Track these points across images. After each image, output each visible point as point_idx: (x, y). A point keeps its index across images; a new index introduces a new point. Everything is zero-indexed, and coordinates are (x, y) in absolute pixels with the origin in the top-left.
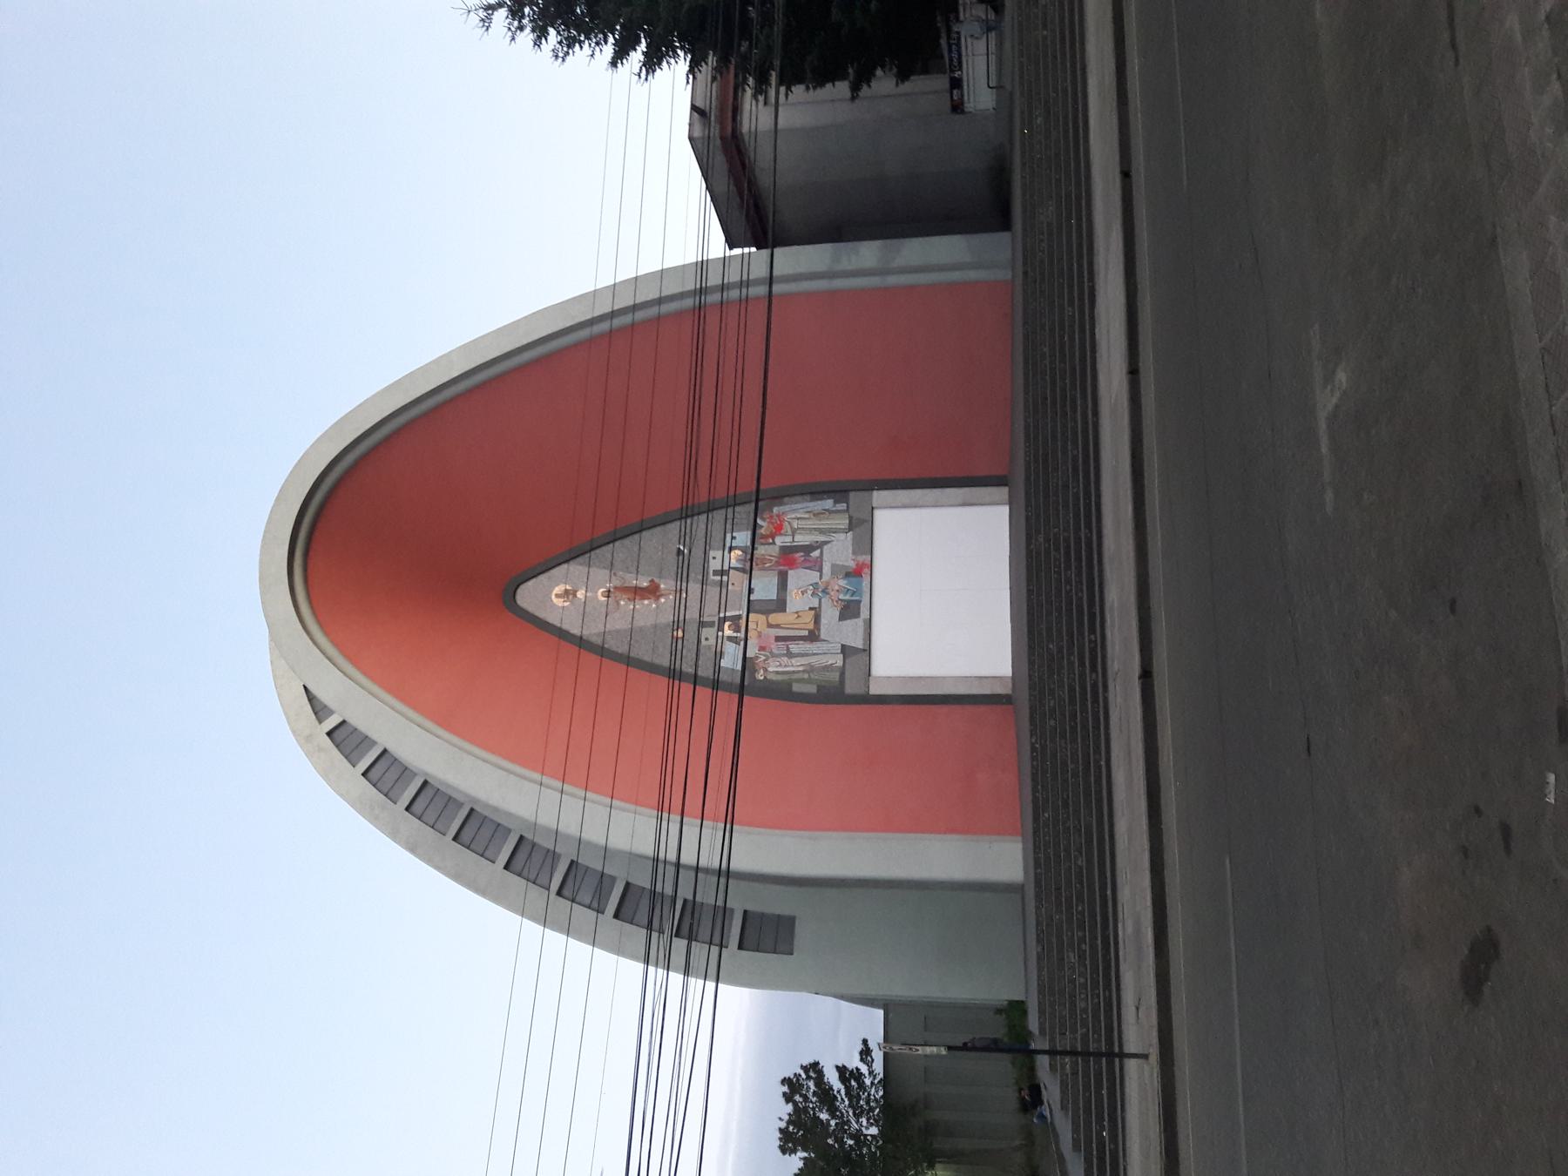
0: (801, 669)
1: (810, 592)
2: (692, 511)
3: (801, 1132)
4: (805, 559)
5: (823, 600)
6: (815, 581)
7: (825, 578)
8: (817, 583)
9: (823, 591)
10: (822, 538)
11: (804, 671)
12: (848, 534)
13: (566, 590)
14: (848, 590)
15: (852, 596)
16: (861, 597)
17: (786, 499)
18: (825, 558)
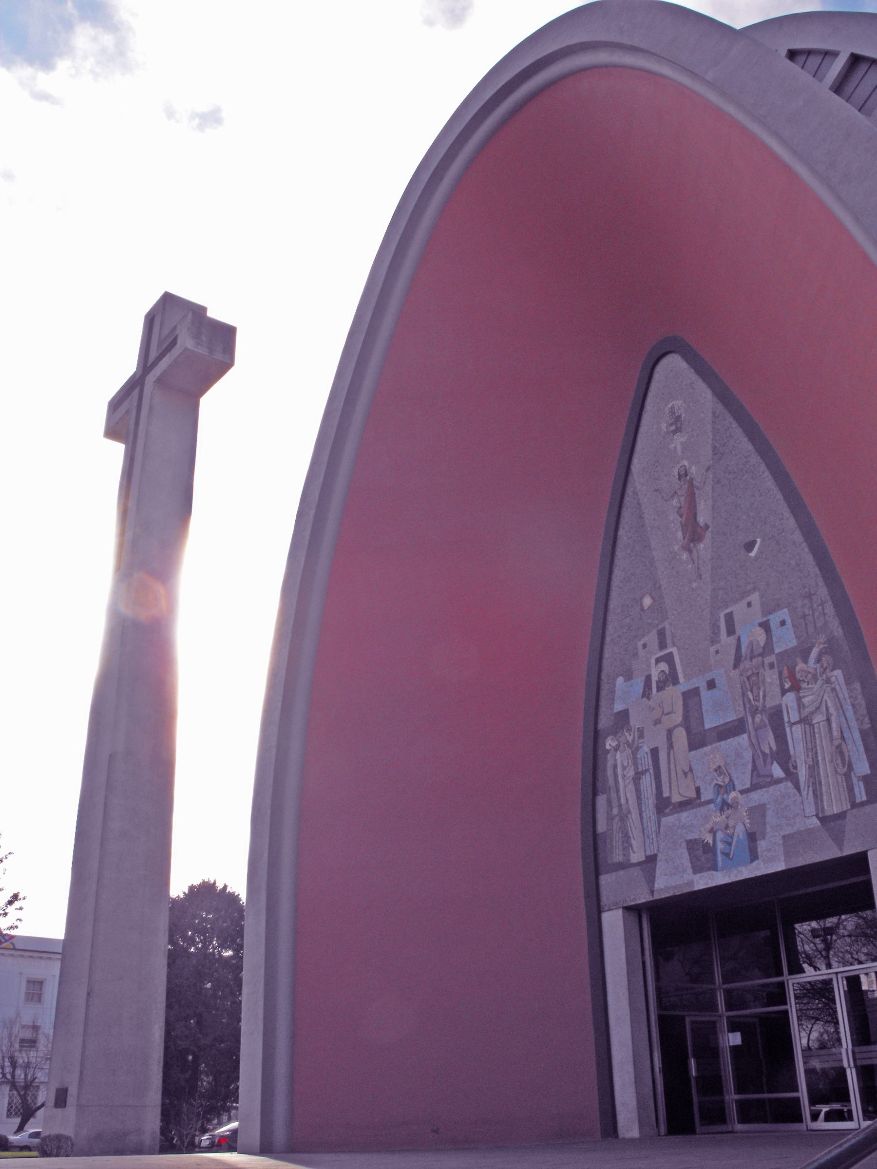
0: (623, 801)
14: (730, 844)
16: (722, 870)
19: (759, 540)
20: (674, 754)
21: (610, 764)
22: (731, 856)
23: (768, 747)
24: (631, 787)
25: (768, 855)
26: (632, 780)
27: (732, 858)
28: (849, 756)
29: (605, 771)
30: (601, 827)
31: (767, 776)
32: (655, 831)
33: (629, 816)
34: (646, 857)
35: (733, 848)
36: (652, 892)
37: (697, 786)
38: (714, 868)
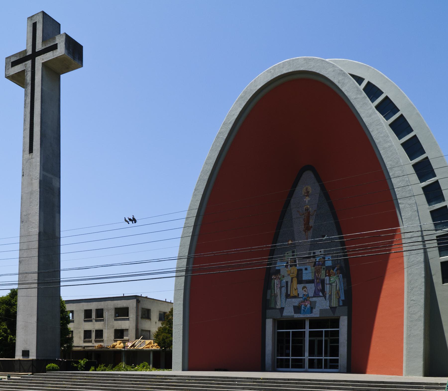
4: (319, 290)
10: (327, 296)
11: (275, 293)
14: (305, 309)
16: (302, 314)
24: (279, 289)
33: (277, 297)
37: (298, 293)
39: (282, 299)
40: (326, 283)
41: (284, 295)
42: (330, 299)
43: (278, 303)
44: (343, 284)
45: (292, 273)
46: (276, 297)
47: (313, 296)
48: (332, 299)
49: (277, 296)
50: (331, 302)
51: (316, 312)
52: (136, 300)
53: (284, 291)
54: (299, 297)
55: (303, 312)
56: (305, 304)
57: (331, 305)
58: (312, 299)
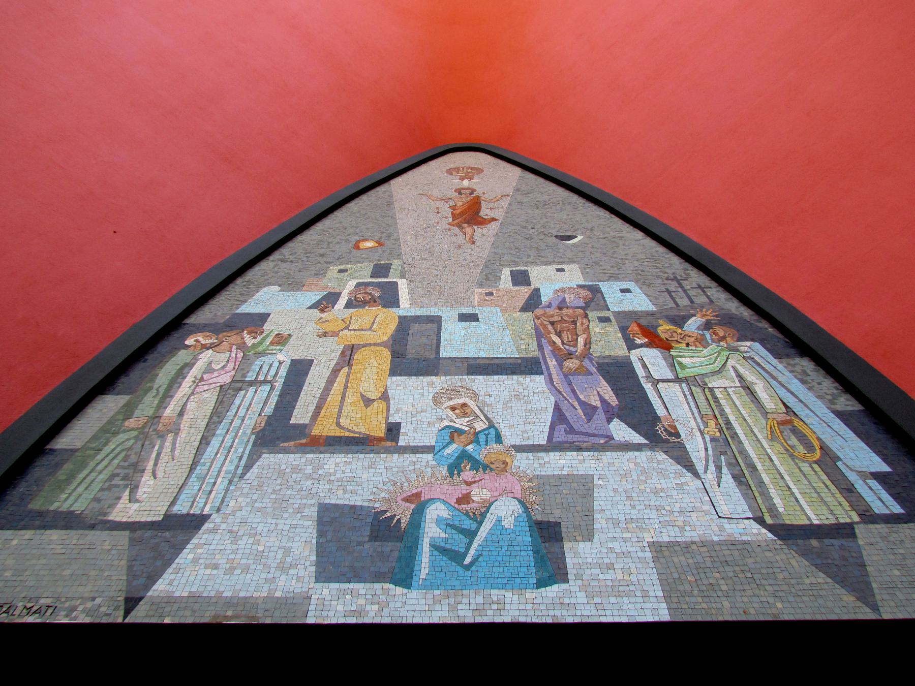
0: (170, 410)
1: (461, 423)
2: (487, 435)
3: (324, 302)
4: (595, 408)
5: (428, 457)
6: (504, 431)
7: (522, 461)
8: (499, 439)
9: (464, 456)
10: (696, 447)
11: (156, 417)
12: (755, 527)
13: (471, 179)
14: (471, 535)
15: (438, 548)
16: (428, 586)
17: (806, 364)
18: (608, 456)
19: (580, 238)
20: (348, 376)
21: (182, 356)
22: (468, 560)
23: (597, 398)
24: (209, 398)
25: (602, 577)
26: (218, 388)
27: (472, 563)
28: (819, 439)
29: (161, 363)
30: (63, 442)
31: (602, 436)
32: (227, 472)
33: (170, 437)
34: (166, 516)
35: (475, 545)
36: (131, 603)
37: (392, 420)
38: (404, 578)
39: (210, 451)
40: (649, 376)
41: (249, 425)
42: (734, 464)
43: (147, 481)
44: (803, 382)
45: (352, 327)
46: (162, 436)
47: (542, 440)
48: (753, 468)
49: (177, 431)
50: (761, 484)
51: (610, 567)
52: (616, 420)
53: (256, 408)
54: (401, 443)
55: (432, 566)
56: (465, 499)
57: (772, 509)
58: (542, 465)
